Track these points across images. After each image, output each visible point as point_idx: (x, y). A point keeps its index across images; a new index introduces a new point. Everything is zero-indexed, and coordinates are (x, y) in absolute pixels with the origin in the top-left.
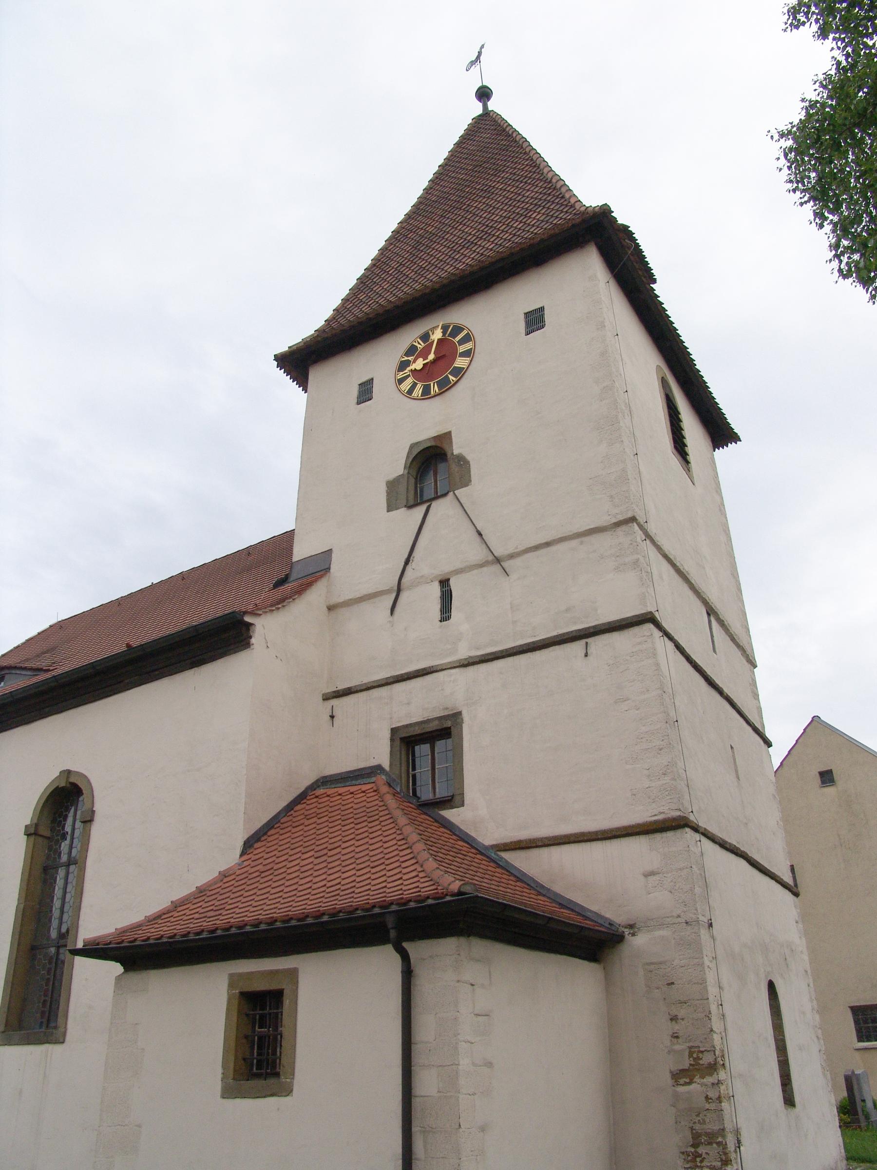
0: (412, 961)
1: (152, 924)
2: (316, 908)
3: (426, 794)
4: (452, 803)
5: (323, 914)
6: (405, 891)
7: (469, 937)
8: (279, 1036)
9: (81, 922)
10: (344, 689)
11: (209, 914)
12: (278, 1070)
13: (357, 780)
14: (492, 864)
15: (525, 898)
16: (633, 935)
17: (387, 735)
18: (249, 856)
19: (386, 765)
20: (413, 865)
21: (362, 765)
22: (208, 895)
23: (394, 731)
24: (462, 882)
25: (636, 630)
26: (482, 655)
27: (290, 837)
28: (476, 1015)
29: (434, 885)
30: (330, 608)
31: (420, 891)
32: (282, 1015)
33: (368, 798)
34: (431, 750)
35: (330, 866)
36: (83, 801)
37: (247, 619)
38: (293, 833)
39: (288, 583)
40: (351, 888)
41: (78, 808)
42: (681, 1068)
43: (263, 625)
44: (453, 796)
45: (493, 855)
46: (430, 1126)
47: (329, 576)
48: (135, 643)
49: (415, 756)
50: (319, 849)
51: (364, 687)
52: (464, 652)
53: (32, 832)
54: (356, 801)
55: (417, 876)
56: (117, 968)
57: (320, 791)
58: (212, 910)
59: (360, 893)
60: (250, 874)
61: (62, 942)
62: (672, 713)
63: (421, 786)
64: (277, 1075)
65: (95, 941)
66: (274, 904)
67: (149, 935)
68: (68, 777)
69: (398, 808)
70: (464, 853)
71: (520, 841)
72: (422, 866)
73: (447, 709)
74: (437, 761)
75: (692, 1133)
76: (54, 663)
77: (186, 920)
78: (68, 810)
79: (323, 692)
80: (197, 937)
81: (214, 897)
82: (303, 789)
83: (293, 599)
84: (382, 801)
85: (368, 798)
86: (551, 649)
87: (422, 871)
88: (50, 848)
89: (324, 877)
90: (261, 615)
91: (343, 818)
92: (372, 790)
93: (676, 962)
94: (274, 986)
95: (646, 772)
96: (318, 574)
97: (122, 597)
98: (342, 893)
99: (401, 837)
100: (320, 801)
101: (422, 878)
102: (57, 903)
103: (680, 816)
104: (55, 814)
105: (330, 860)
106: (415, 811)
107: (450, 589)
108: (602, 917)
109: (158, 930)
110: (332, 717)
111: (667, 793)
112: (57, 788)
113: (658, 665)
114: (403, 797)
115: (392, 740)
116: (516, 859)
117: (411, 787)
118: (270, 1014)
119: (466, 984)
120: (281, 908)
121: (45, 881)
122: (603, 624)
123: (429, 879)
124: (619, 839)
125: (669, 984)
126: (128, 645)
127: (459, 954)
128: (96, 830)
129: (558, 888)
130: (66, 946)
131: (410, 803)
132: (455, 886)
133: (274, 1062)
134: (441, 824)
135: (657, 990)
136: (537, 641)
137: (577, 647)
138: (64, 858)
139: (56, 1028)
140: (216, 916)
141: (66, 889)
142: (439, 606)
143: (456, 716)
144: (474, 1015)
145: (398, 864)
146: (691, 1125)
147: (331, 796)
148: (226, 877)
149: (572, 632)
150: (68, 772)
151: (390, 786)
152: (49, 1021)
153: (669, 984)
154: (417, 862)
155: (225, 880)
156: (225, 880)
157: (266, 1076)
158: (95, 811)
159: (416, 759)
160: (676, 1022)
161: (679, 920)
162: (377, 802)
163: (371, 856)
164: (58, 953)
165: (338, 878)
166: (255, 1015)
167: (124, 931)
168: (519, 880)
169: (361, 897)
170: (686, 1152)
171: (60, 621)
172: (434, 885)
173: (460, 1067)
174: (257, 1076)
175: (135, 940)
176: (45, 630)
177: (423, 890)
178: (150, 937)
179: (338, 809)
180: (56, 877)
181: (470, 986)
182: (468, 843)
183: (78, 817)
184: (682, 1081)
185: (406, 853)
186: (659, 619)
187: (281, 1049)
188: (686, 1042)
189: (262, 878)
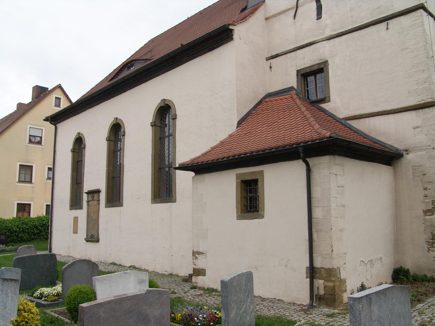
0: (310, 166)
1: (204, 156)
2: (269, 146)
3: (313, 98)
4: (325, 101)
5: (273, 148)
6: (306, 137)
7: (334, 155)
8: (257, 197)
9: (176, 158)
10: (275, 55)
11: (226, 151)
12: (258, 209)
13: (283, 94)
14: (343, 126)
15: (358, 140)
16: (407, 154)
17: (295, 73)
18: (240, 128)
19: (295, 86)
20: (309, 127)
21: (285, 87)
22: (225, 144)
23: (298, 71)
24: (331, 133)
25: (414, 14)
26: (337, 34)
27: (261, 118)
28: (338, 187)
29: (318, 134)
30: (266, 19)
31: (313, 137)
32: (258, 189)
33: (288, 101)
34: (315, 78)
35: (274, 129)
36: (171, 111)
37: (231, 27)
38: (257, 117)
39: (247, 9)
40: (284, 137)
41: (170, 114)
42: (428, 209)
43: (238, 30)
44: (325, 98)
45: (344, 122)
46: (320, 229)
47: (265, 4)
48: (184, 43)
49: (308, 82)
50: (242, 138)
51: (284, 53)
52: (328, 33)
53: (153, 125)
54: (283, 102)
55: (311, 131)
56: (192, 174)
57: (267, 100)
58: (227, 150)
59: (287, 139)
60: (241, 135)
61: (170, 166)
62: (431, 53)
63: (311, 94)
64: (258, 211)
65: (183, 163)
66: (252, 146)
67: (203, 160)
68: (164, 102)
69: (301, 104)
70: (331, 122)
71: (356, 116)
72: (313, 127)
73: (321, 59)
74: (317, 83)
75: (432, 234)
76: (152, 56)
77: (217, 154)
78: (166, 115)
79: (266, 57)
80: (222, 160)
81: (233, 141)
82: (260, 99)
83: (250, 17)
84: (294, 102)
85: (288, 101)
86: (370, 27)
87: (313, 129)
88: (161, 130)
89: (272, 134)
90: (236, 25)
91: (278, 110)
92: (290, 97)
93: (427, 165)
94: (254, 178)
95: (416, 82)
96: (261, 3)
97: (176, 25)
98: (279, 140)
99: (303, 116)
100: (268, 103)
101: (313, 132)
102: (167, 152)
103: (432, 101)
104: (161, 117)
105: (279, 126)
106: (309, 105)
107: (321, 4)
108: (393, 147)
109: (207, 158)
110: (271, 67)
111: (426, 91)
112: (161, 106)
113: (424, 30)
114: (303, 99)
115: (297, 75)
116: (354, 123)
117: (306, 95)
118: (253, 189)
119: (333, 175)
120: (255, 147)
121: (161, 144)
122: (397, 13)
123: (316, 132)
124: (401, 113)
125: (423, 175)
126: (182, 45)
127: (330, 162)
128: (178, 121)
129: (373, 135)
130: (172, 167)
131: (306, 102)
132: (328, 135)
133: (256, 206)
134: (321, 110)
135: (418, 177)
136: (363, 25)
137: (383, 26)
138: (167, 134)
139: (172, 197)
140: (229, 152)
141: (169, 146)
142: (316, 13)
143: (326, 63)
144: (337, 187)
145: (302, 127)
146: (431, 231)
147: (272, 101)
148: (231, 136)
149: (380, 18)
150: (164, 100)
151: (297, 95)
152: (169, 195)
153: (423, 175)
154: (311, 126)
155: (231, 138)
156: (231, 138)
157: (254, 212)
158: (176, 114)
159: (308, 83)
160: (426, 190)
161: (430, 147)
162: (292, 102)
163: (291, 125)
164: (169, 170)
165: (277, 134)
166: (247, 189)
167: (193, 160)
168: (355, 132)
169: (287, 141)
170: (429, 241)
171: (152, 39)
172: (318, 134)
173: (332, 207)
174: (250, 212)
175: (198, 162)
176: (147, 43)
177: (314, 137)
178: (209, 160)
179: (281, 105)
180: (165, 142)
181: (335, 175)
182: (332, 118)
183: (170, 117)
184: (428, 214)
185: (306, 122)
186: (426, 6)
187: (258, 201)
188: (431, 199)
189: (246, 136)
